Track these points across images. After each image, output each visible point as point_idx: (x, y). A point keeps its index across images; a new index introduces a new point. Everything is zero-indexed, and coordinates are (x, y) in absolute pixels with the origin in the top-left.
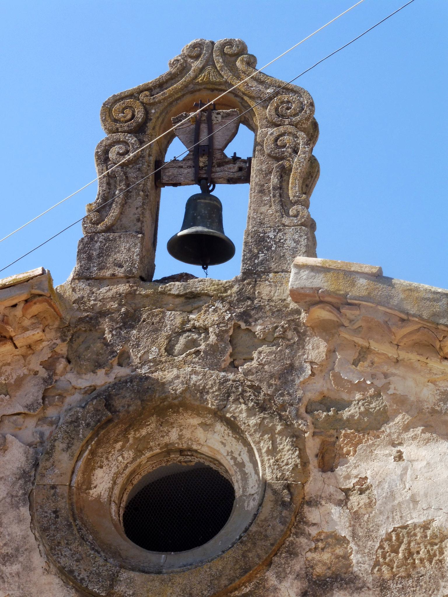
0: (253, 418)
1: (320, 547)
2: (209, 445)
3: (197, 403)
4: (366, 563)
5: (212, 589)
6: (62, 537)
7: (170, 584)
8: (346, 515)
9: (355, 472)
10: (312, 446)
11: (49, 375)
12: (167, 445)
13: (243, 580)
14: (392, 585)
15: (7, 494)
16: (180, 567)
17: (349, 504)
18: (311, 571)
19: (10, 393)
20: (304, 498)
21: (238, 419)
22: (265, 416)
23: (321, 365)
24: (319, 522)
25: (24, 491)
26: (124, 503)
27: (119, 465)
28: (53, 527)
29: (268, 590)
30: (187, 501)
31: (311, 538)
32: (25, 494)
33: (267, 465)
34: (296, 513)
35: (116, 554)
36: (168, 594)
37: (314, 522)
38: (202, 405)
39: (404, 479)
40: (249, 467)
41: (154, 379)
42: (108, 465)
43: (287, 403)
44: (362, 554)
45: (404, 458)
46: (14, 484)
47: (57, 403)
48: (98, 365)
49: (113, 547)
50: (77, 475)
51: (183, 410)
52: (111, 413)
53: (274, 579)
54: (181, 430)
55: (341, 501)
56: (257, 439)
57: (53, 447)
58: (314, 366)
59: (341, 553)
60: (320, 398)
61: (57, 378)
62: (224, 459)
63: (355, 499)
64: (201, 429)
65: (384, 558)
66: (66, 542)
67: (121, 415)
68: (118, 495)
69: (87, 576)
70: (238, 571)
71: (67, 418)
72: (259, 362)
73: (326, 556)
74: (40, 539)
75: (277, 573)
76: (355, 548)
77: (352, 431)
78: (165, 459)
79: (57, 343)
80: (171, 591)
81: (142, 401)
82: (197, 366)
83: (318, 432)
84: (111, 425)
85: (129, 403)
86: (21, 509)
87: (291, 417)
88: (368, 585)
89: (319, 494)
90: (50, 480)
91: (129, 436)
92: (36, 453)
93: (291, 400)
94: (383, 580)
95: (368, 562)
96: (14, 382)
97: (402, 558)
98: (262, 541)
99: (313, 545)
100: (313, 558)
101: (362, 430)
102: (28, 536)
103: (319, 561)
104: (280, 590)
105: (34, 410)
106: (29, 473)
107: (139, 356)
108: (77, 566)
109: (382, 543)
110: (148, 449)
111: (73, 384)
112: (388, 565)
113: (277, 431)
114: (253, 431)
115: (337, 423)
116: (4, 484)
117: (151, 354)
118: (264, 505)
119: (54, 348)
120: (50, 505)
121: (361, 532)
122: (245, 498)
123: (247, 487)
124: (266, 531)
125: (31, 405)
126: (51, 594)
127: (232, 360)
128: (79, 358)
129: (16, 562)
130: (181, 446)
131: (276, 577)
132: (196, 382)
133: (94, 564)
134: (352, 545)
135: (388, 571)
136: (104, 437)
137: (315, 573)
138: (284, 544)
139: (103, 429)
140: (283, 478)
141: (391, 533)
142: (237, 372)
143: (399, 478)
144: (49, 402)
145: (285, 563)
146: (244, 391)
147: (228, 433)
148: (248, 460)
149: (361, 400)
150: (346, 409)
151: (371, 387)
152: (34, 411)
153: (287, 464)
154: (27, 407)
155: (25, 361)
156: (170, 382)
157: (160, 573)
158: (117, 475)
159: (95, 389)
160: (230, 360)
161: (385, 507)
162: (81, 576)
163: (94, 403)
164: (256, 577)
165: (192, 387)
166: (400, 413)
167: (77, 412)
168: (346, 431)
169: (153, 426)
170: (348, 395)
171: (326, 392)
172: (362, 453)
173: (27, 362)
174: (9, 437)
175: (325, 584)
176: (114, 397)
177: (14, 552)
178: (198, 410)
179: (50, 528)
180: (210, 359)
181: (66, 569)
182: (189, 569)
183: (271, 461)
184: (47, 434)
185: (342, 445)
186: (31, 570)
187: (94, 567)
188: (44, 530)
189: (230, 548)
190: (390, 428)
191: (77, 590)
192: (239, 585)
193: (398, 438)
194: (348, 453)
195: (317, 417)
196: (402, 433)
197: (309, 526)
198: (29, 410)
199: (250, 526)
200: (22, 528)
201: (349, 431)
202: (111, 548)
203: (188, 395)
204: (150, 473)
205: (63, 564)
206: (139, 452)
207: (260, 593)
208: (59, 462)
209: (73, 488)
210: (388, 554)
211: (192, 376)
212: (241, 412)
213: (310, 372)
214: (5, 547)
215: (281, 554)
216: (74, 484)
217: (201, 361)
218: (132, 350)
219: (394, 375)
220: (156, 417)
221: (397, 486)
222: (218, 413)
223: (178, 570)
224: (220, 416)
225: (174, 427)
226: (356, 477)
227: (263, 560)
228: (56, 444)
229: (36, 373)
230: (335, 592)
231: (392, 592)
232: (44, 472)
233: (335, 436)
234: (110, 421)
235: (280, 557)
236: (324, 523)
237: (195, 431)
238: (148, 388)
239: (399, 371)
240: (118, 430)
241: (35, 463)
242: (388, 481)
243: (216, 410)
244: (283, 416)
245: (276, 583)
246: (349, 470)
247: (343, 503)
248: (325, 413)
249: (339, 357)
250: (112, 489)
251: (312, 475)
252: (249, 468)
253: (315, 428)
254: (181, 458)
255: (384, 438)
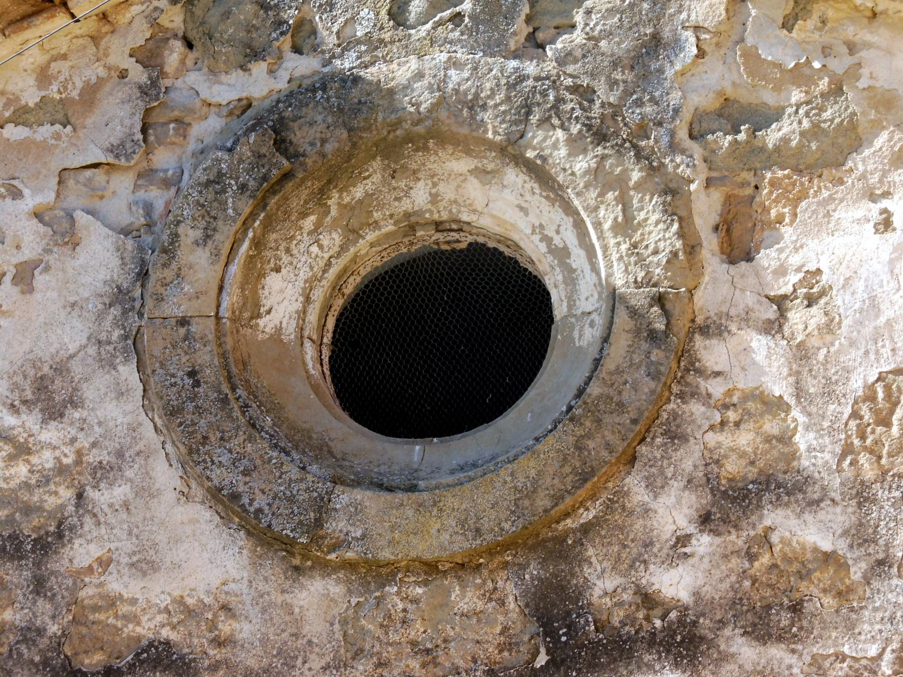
0: (581, 157)
1: (731, 419)
2: (494, 212)
3: (465, 130)
4: (827, 450)
5: (519, 517)
6: (210, 425)
7: (435, 512)
8: (782, 352)
9: (795, 260)
10: (706, 208)
11: (150, 78)
12: (407, 215)
13: (581, 496)
14: (880, 493)
15: (89, 339)
16: (452, 472)
17: (786, 328)
18: (716, 470)
19: (73, 120)
20: (693, 321)
21: (550, 161)
22: (606, 151)
23: (718, 34)
24: (727, 369)
25: (122, 332)
26: (330, 335)
27: (313, 264)
28: (190, 406)
29: (631, 513)
30: (457, 321)
31: (712, 402)
32: (125, 337)
33: (615, 257)
34: (680, 353)
35: (321, 451)
36: (433, 531)
37: (717, 369)
38: (475, 134)
39: (896, 271)
40: (579, 256)
41: (370, 83)
42: (291, 263)
43: (650, 120)
44: (817, 431)
45: (895, 225)
46: (100, 317)
47: (173, 139)
48: (253, 53)
49: (314, 436)
50: (229, 294)
51: (435, 144)
52: (288, 159)
53: (642, 490)
54: (435, 185)
55: (770, 322)
56: (592, 203)
57: (175, 236)
58: (704, 36)
59: (775, 431)
60: (718, 105)
61: (167, 82)
62: (527, 240)
63: (799, 318)
64: (475, 181)
65: (863, 437)
66: (219, 435)
67: (309, 162)
68: (315, 324)
69: (269, 504)
70: (569, 479)
71: (198, 173)
72: (587, 34)
73: (745, 439)
74: (165, 431)
75: (647, 478)
76: (802, 419)
77: (786, 172)
78: (406, 240)
79: (161, 7)
80: (438, 526)
81: (350, 130)
82: (458, 48)
83: (716, 179)
84: (290, 184)
85: (323, 136)
86: (121, 368)
87: (659, 149)
88: (833, 495)
89: (724, 309)
90: (174, 307)
91: (329, 202)
92: (141, 249)
93: (658, 114)
94: (862, 483)
95: (829, 448)
96: (79, 95)
97: (898, 435)
98: (614, 415)
99: (718, 418)
100: (717, 443)
101: (806, 169)
102: (140, 424)
103: (732, 450)
104: (656, 512)
105: (128, 157)
106: (129, 292)
107: (335, 29)
108: (246, 483)
109: (856, 407)
110: (369, 225)
111: (203, 95)
112: (872, 452)
113: (631, 183)
114: (582, 185)
115: (755, 157)
116: (79, 316)
117: (360, 24)
118: (612, 339)
119: (155, 19)
120: (180, 359)
121: (814, 386)
122: (573, 320)
123: (575, 297)
124: (620, 393)
125: (119, 146)
126: (197, 544)
127: (531, 30)
128: (210, 39)
129: (119, 481)
130: (436, 217)
131: (647, 486)
132: (459, 84)
133: (280, 477)
134: (795, 413)
135: (872, 464)
136: (278, 209)
137: (723, 473)
138: (657, 418)
139: (275, 193)
140: (648, 281)
141: (873, 384)
142: (542, 58)
143: (886, 269)
144: (156, 137)
145: (662, 457)
146: (559, 100)
147: (532, 188)
148: (576, 242)
149: (801, 104)
150: (773, 126)
151: (822, 74)
152: (127, 160)
153: (656, 252)
154: (111, 150)
155: (97, 48)
156: (405, 87)
157: (413, 488)
158: (311, 283)
159: (249, 106)
160: (526, 30)
161: (859, 332)
162: (256, 505)
163: (251, 141)
164: (606, 488)
165: (451, 96)
166: (884, 128)
167: (219, 161)
168: (774, 173)
169: (377, 178)
170: (775, 94)
171: (730, 92)
172: (809, 218)
173: (101, 52)
174: (81, 218)
175: (746, 497)
176: (291, 124)
177: (113, 460)
178: (469, 144)
179: (183, 408)
180: (484, 32)
181: (225, 492)
182: (471, 479)
183: (624, 247)
184: (159, 206)
185: (767, 203)
186: (152, 496)
187: (280, 485)
188: (172, 412)
189: (551, 431)
190: (864, 161)
191: (249, 533)
192: (573, 506)
193: (881, 181)
194: (780, 220)
195: (714, 146)
196: (890, 170)
197: (707, 378)
198: (117, 156)
199: (587, 383)
200: (125, 408)
201: (780, 173)
202: (310, 438)
203: (443, 114)
204: (377, 268)
205: (216, 482)
206: (352, 234)
207: (616, 521)
208: (191, 268)
209: (224, 320)
210: (869, 429)
211: (449, 72)
212: (555, 146)
213: (695, 51)
214: (94, 451)
215: (653, 439)
216: (225, 313)
217: (465, 37)
218: (320, 17)
219: (868, 45)
220: (382, 160)
221: (882, 286)
222: (510, 149)
223: (450, 479)
224: (514, 156)
225: (419, 179)
226: (799, 270)
227: (618, 455)
228: (181, 230)
229: (123, 74)
230: (766, 512)
231: (882, 507)
232: (161, 290)
233: (753, 185)
234: (287, 176)
235: (652, 444)
236: (737, 370)
237: (463, 185)
238: (360, 101)
239: (877, 36)
240: (306, 192)
241: (141, 270)
242: (863, 277)
243: (504, 144)
244: (643, 149)
245: (646, 498)
246: (783, 256)
247: (774, 328)
248: (729, 138)
249: (753, 12)
250: (303, 313)
251: (708, 270)
252: (578, 258)
253: (710, 169)
254: (440, 236)
255: (853, 183)
